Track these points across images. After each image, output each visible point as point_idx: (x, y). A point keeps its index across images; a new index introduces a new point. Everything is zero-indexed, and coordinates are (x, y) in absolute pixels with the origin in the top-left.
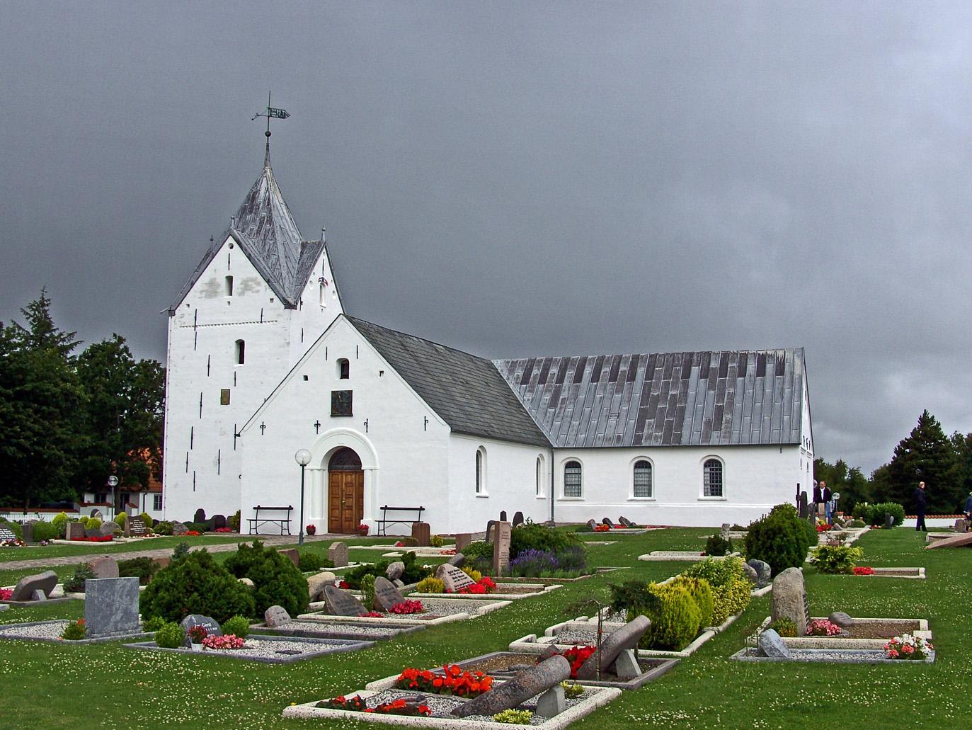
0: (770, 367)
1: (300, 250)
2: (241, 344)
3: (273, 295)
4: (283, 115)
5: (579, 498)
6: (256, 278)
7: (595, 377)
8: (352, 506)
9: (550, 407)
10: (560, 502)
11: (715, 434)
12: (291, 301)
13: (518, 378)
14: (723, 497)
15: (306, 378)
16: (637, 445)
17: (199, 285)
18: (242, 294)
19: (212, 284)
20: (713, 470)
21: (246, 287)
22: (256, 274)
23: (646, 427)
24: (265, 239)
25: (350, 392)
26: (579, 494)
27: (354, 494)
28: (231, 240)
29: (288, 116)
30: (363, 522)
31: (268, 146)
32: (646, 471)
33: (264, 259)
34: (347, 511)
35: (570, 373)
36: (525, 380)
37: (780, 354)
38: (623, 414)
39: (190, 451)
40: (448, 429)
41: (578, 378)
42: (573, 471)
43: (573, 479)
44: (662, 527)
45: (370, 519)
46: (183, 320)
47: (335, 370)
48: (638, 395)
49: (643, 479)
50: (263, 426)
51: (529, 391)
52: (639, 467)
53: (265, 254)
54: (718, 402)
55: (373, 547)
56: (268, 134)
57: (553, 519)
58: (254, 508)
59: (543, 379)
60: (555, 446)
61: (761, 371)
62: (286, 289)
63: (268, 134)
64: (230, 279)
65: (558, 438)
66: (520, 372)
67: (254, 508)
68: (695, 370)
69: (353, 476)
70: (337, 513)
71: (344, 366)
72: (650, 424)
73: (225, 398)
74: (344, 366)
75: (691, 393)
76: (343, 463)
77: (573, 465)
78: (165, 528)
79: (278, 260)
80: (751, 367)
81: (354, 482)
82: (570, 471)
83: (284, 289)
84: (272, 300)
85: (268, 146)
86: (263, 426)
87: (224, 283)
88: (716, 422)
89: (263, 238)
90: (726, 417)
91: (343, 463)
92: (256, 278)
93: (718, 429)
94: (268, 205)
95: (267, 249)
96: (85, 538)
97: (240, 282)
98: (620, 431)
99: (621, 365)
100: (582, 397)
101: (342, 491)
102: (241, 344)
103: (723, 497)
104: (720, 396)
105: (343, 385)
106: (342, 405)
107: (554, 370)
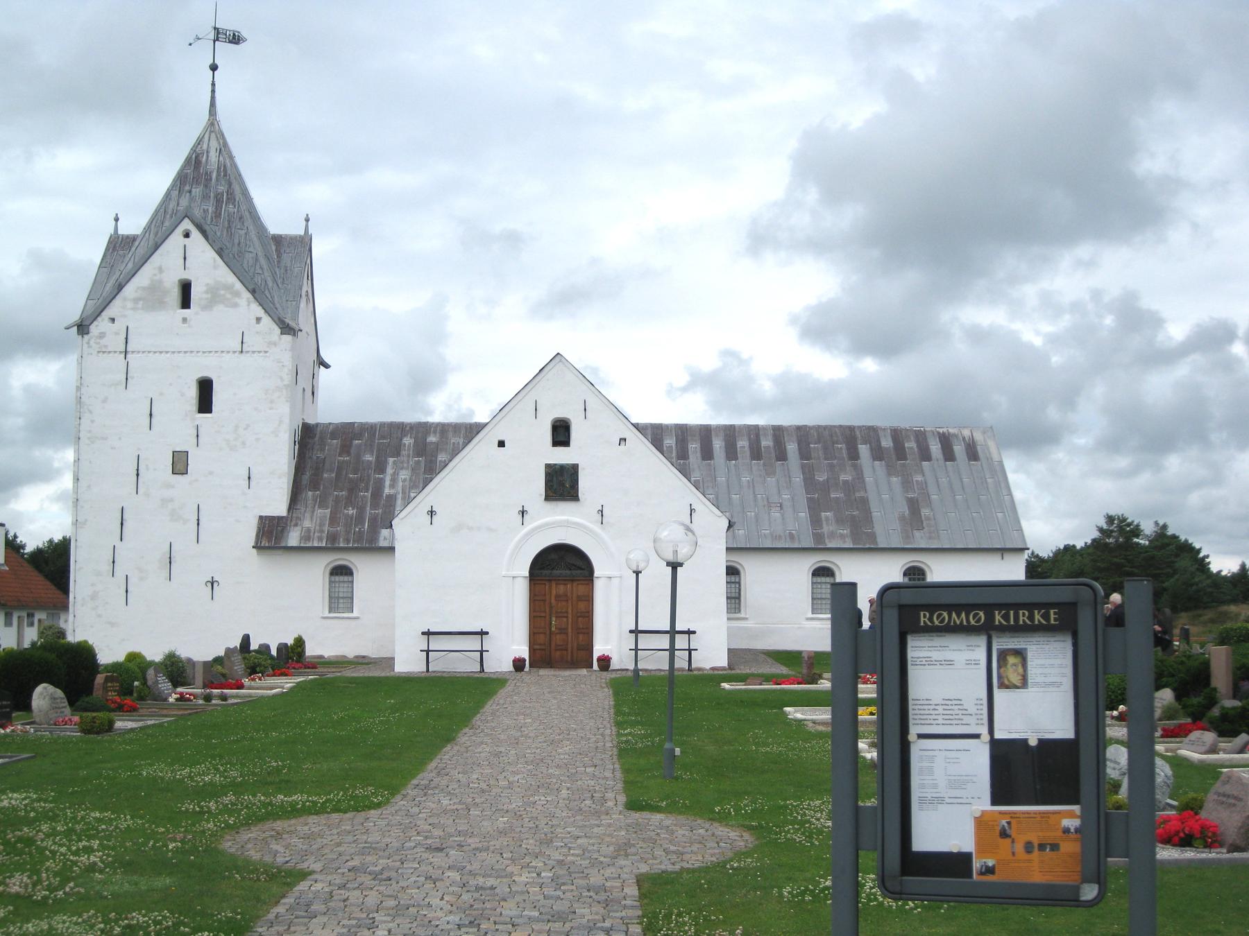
0: (959, 449)
2: (205, 389)
3: (260, 312)
4: (236, 39)
5: (350, 615)
6: (232, 286)
14: (355, 614)
15: (501, 444)
16: (332, 546)
17: (130, 290)
18: (208, 306)
21: (216, 296)
22: (231, 279)
24: (230, 227)
25: (575, 468)
28: (187, 225)
29: (245, 40)
31: (213, 84)
32: (346, 578)
35: (694, 447)
37: (966, 433)
38: (787, 504)
46: (103, 342)
48: (798, 479)
53: (235, 249)
56: (214, 68)
61: (949, 455)
63: (214, 68)
64: (186, 288)
67: (423, 633)
68: (864, 450)
71: (561, 433)
73: (180, 464)
74: (561, 433)
75: (869, 480)
76: (561, 576)
80: (935, 448)
84: (258, 320)
87: (175, 294)
88: (914, 516)
90: (925, 512)
91: (561, 576)
94: (225, 175)
95: (236, 241)
97: (204, 289)
100: (722, 480)
101: (551, 607)
102: (205, 389)
103: (355, 614)
104: (907, 484)
105: (562, 456)
106: (562, 484)
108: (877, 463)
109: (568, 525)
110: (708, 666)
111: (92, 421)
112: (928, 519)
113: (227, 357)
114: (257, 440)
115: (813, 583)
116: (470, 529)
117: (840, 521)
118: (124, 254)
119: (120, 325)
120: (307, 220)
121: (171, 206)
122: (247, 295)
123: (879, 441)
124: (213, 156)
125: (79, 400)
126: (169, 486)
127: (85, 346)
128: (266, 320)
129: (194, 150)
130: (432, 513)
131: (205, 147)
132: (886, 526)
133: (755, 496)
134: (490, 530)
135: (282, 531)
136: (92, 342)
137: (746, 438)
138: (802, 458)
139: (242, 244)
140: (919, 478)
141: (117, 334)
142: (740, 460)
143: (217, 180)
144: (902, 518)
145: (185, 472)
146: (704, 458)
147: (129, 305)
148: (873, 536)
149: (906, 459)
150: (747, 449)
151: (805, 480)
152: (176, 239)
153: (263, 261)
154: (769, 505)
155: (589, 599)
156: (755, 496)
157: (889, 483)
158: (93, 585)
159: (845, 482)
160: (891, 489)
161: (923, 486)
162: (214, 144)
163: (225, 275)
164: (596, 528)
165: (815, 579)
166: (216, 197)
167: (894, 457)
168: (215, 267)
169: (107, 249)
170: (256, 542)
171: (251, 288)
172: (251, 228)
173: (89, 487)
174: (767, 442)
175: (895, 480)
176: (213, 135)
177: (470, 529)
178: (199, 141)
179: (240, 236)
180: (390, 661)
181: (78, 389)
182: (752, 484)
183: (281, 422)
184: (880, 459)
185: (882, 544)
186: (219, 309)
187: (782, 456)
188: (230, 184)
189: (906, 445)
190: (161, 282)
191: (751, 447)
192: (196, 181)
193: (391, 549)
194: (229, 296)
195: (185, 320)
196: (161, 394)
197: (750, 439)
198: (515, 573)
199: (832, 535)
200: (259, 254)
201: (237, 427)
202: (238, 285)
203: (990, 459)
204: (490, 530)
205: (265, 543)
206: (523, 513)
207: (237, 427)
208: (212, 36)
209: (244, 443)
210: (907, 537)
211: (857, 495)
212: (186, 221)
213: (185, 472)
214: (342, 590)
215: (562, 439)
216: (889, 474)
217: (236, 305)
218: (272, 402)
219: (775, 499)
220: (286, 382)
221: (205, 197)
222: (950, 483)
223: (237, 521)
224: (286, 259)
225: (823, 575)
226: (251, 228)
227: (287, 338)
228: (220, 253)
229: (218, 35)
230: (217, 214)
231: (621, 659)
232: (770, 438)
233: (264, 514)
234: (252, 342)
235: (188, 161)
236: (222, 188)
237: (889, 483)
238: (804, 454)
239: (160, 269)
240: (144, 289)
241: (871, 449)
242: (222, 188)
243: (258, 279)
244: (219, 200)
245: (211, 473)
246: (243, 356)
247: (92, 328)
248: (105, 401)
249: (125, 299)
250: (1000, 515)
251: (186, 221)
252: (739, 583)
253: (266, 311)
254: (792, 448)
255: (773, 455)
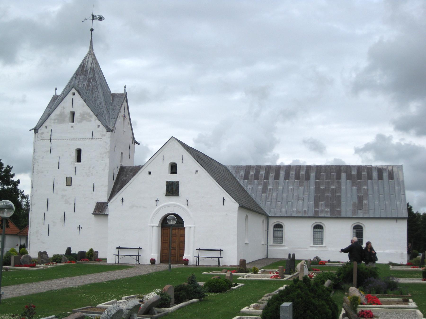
0: (385, 175)
1: (111, 98)
2: (79, 152)
3: (99, 123)
6: (90, 113)
7: (287, 177)
8: (176, 248)
9: (263, 193)
10: (311, 248)
11: (359, 211)
12: (111, 128)
13: (242, 176)
14: (324, 245)
15: (150, 173)
18: (80, 122)
19: (62, 115)
20: (358, 231)
21: (83, 118)
22: (89, 111)
23: (320, 206)
24: (92, 91)
26: (282, 242)
27: (177, 241)
28: (73, 90)
30: (184, 257)
31: (92, 37)
32: (320, 230)
33: (92, 103)
34: (172, 251)
35: (272, 174)
36: (246, 177)
39: (46, 212)
40: (237, 205)
41: (277, 177)
42: (278, 229)
43: (279, 234)
44: (338, 262)
45: (189, 254)
46: (43, 136)
47: (167, 168)
48: (313, 188)
49: (318, 235)
50: (122, 200)
51: (250, 184)
52: (316, 228)
53: (93, 99)
54: (359, 193)
55: (211, 273)
57: (267, 256)
58: (117, 248)
59: (256, 177)
60: (269, 215)
61: (380, 177)
62: (107, 120)
63: (92, 30)
64: (73, 114)
65: (270, 210)
66: (242, 173)
67: (117, 248)
68: (343, 175)
69: (177, 231)
70: (166, 251)
71: (173, 169)
72: (322, 204)
73: (69, 182)
74: (173, 169)
75: (343, 188)
76: (172, 230)
77: (279, 226)
78: (58, 259)
79: (101, 103)
80: (375, 175)
81: (177, 234)
82: (276, 229)
83: (105, 120)
84: (99, 126)
85: (92, 37)
86: (122, 200)
87: (69, 116)
88: (360, 204)
89: (91, 89)
90: (365, 202)
91: (172, 230)
92: (90, 113)
93: (361, 208)
94: (93, 71)
95: (94, 96)
96: (20, 265)
98: (306, 208)
99: (301, 171)
100: (280, 188)
102: (79, 152)
103: (324, 245)
104: (359, 190)
105: (173, 178)
106: (172, 189)
107: (262, 173)
108: (348, 181)
109: (174, 205)
110: (229, 265)
111: (38, 166)
112: (366, 205)
113: (87, 141)
114: (97, 172)
115: (314, 232)
116: (137, 207)
117: (327, 206)
118: (56, 101)
119: (49, 129)
120: (125, 87)
121: (72, 83)
122: (94, 117)
123: (351, 172)
124: (89, 64)
125: (34, 158)
126: (64, 190)
127: (36, 137)
128: (101, 126)
129: (83, 62)
130: (122, 200)
131: (87, 60)
132: (346, 207)
133: (293, 195)
134: (144, 207)
135: (104, 208)
136: (39, 136)
137: (294, 171)
138: (316, 179)
139: (96, 97)
140: (365, 187)
141: (48, 132)
142: (290, 180)
143: (90, 73)
144: (354, 205)
145: (70, 185)
146: (275, 179)
147: (52, 121)
148: (340, 212)
149: (361, 179)
150: (294, 176)
151: (315, 188)
152: (70, 96)
153: (103, 103)
154: (298, 198)
155: (183, 236)
156: (293, 195)
157: (352, 189)
158: (37, 227)
159: (333, 189)
160: (352, 192)
161: (367, 191)
162: (90, 59)
163: (87, 110)
164: (185, 207)
165: (315, 230)
166: (88, 79)
167: (356, 178)
168: (83, 106)
169: (51, 100)
170: (94, 212)
171: (96, 114)
172: (100, 91)
173: (36, 190)
174: (303, 173)
175: (354, 188)
176: (90, 56)
177: (137, 207)
178: (85, 59)
179: (96, 94)
180: (105, 260)
181: (34, 153)
182: (293, 190)
183: (106, 166)
184: (350, 179)
185: (343, 215)
186: (84, 122)
187: (308, 178)
188: (94, 74)
189: (363, 173)
190: (64, 112)
191: (295, 174)
192: (82, 73)
193: (107, 215)
194: (88, 117)
195: (72, 127)
196: (63, 155)
197: (296, 172)
198: (153, 225)
199: (322, 212)
200: (102, 101)
201: (90, 168)
202: (92, 113)
203: (398, 179)
204: (144, 207)
205: (97, 212)
206: (157, 201)
207: (90, 168)
208: (91, 18)
209: (92, 174)
210: (354, 212)
211: (337, 194)
212: (73, 89)
213: (70, 185)
214: (279, 234)
215: (174, 171)
216: (353, 185)
217: (90, 121)
218: (103, 158)
219: (301, 196)
220: (108, 150)
221: (84, 80)
222: (378, 189)
223: (89, 204)
224: (115, 102)
225: (318, 228)
226: (100, 91)
227: (109, 133)
228: (85, 100)
229: (94, 17)
230: (88, 86)
231: (192, 261)
232: (305, 171)
233: (99, 201)
234: (96, 135)
235: (80, 66)
236: (91, 76)
237: (352, 189)
238: (318, 177)
239: (64, 108)
240: (58, 115)
241: (347, 175)
242: (91, 76)
243: (100, 111)
244: (89, 80)
245: (80, 185)
246: (93, 140)
247: (39, 130)
248: (43, 158)
249: (51, 119)
250: (398, 203)
251: (73, 89)
252: (283, 231)
253: (101, 123)
254: (313, 175)
255: (304, 178)
